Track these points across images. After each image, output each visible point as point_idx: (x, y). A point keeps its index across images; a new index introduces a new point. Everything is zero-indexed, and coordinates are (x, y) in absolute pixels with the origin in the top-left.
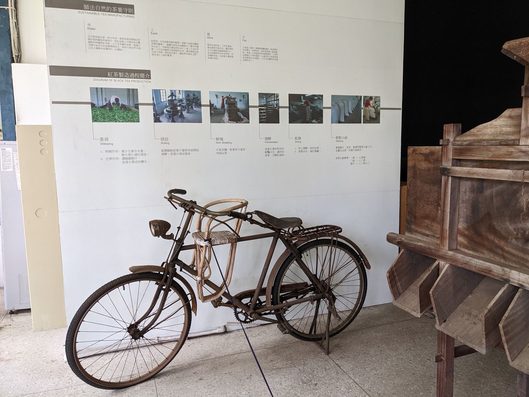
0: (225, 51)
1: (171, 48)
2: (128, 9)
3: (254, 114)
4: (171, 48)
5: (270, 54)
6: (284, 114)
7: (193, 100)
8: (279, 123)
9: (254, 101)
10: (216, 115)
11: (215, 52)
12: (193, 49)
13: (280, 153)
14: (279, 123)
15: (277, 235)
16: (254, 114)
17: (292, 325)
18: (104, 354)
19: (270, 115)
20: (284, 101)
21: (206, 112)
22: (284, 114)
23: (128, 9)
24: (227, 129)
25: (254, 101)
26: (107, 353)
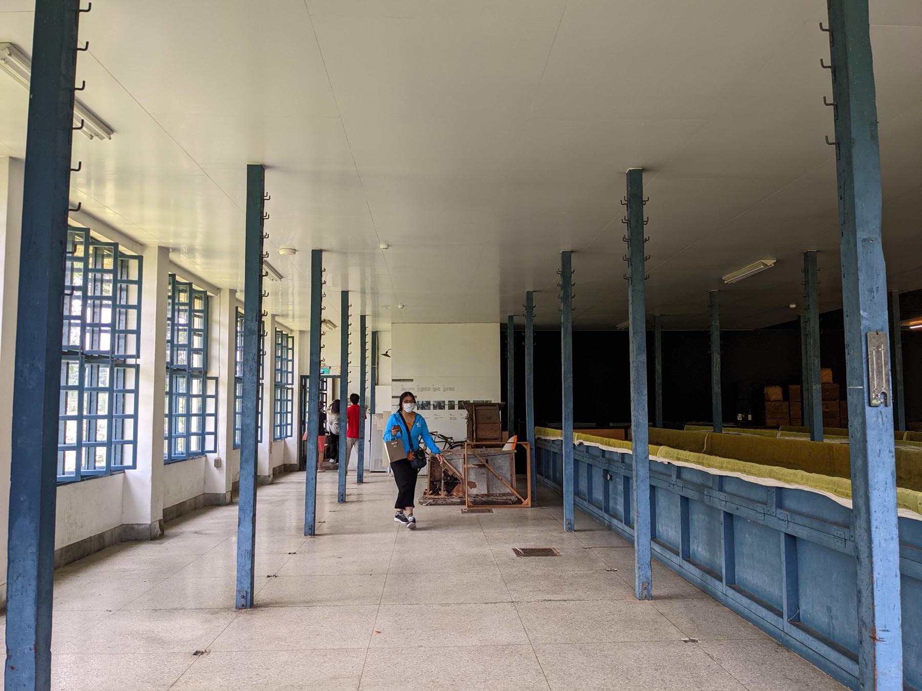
0: (439, 389)
1: (423, 389)
2: (412, 380)
3: (447, 407)
4: (423, 389)
5: (452, 389)
6: (456, 407)
7: (428, 403)
8: (248, 166)
9: (447, 403)
10: (435, 407)
11: (435, 390)
12: (429, 389)
13: (455, 419)
14: (248, 166)
15: (446, 441)
16: (447, 407)
17: (71, 222)
18: (749, 619)
19: (452, 407)
20: (456, 403)
21: (432, 407)
22: (456, 407)
23: (412, 380)
24: (438, 411)
25: (447, 403)
26: (755, 623)
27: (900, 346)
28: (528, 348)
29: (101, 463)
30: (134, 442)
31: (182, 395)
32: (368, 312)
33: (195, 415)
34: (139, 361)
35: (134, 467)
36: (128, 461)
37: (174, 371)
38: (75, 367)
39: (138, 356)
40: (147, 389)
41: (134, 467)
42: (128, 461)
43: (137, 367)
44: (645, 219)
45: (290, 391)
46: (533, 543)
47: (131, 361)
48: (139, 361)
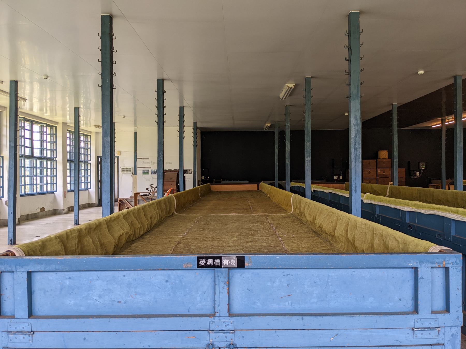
2: (148, 158)
23: (148, 158)
27: (397, 136)
28: (211, 142)
29: (49, 189)
30: (90, 182)
31: (45, 168)
32: (430, 265)
33: (27, 176)
34: (56, 159)
35: (91, 188)
36: (89, 187)
37: (51, 159)
38: (83, 164)
39: (91, 161)
40: (93, 169)
41: (56, 191)
42: (89, 187)
43: (90, 163)
44: (361, 31)
45: (89, 165)
46: (51, 278)
47: (89, 162)
48: (56, 159)
